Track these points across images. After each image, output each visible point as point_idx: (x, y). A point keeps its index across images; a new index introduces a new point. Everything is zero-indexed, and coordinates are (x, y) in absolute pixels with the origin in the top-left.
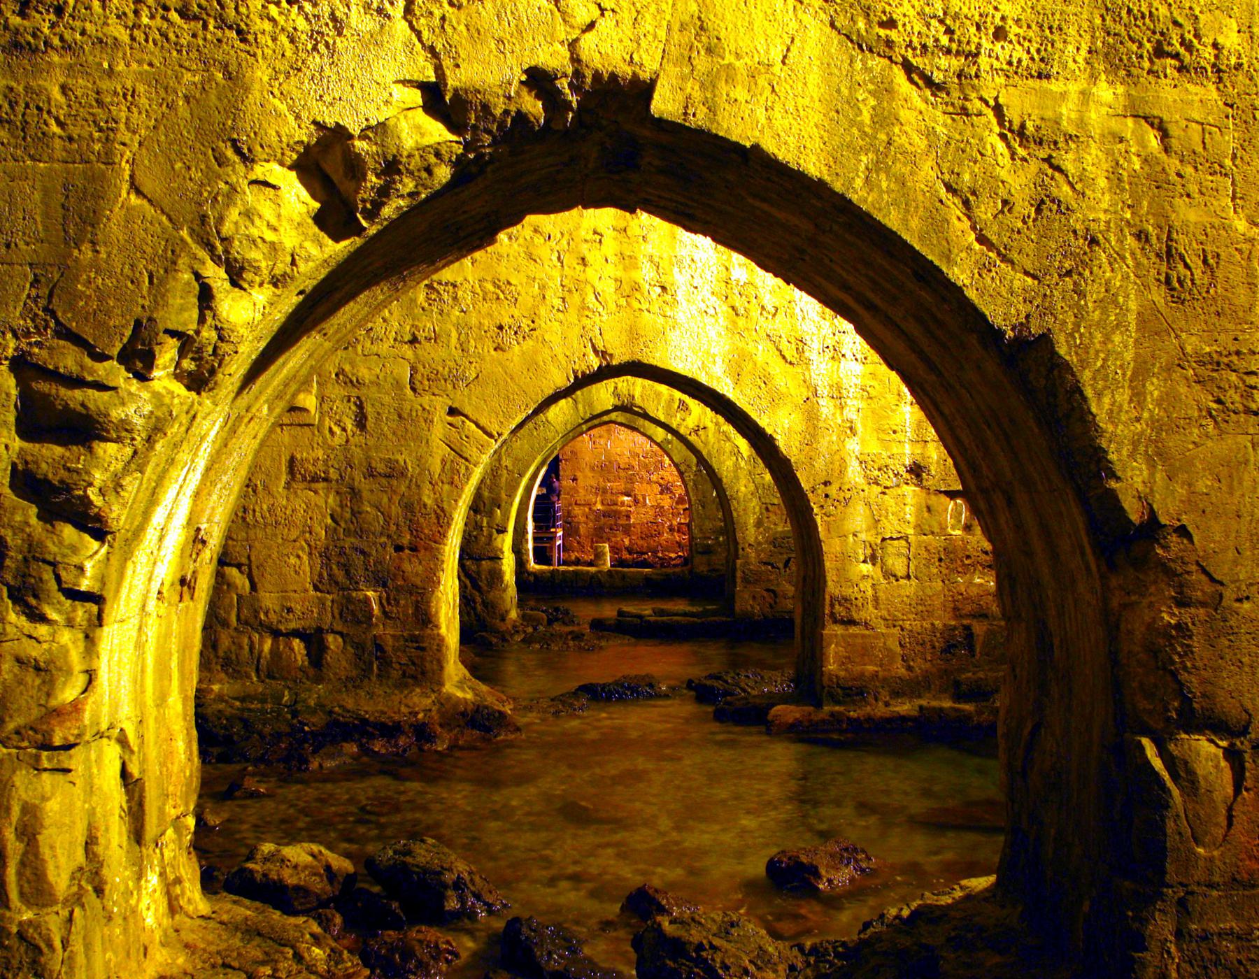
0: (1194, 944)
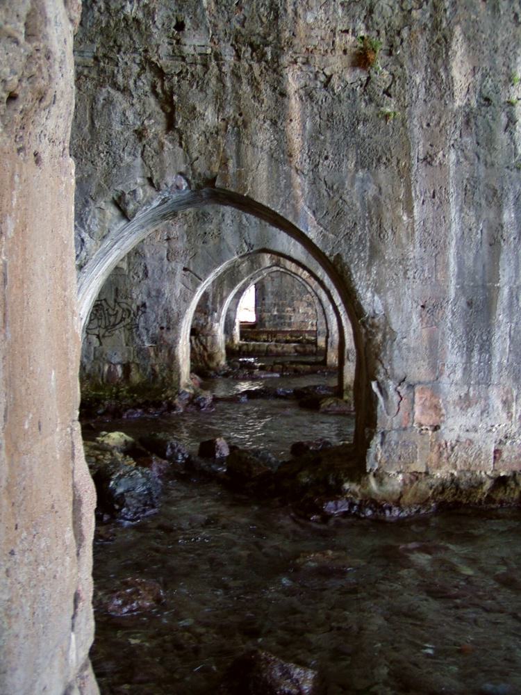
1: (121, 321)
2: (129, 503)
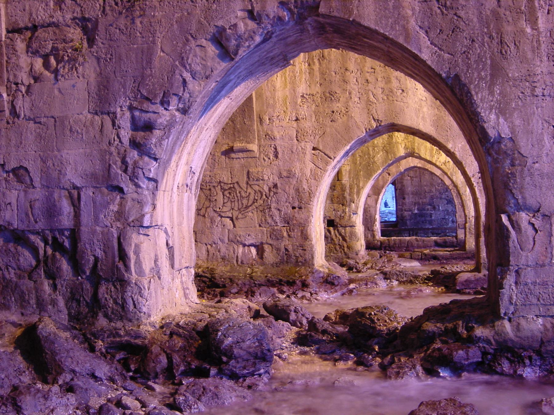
0: (522, 287)
1: (254, 202)
2: (237, 356)
